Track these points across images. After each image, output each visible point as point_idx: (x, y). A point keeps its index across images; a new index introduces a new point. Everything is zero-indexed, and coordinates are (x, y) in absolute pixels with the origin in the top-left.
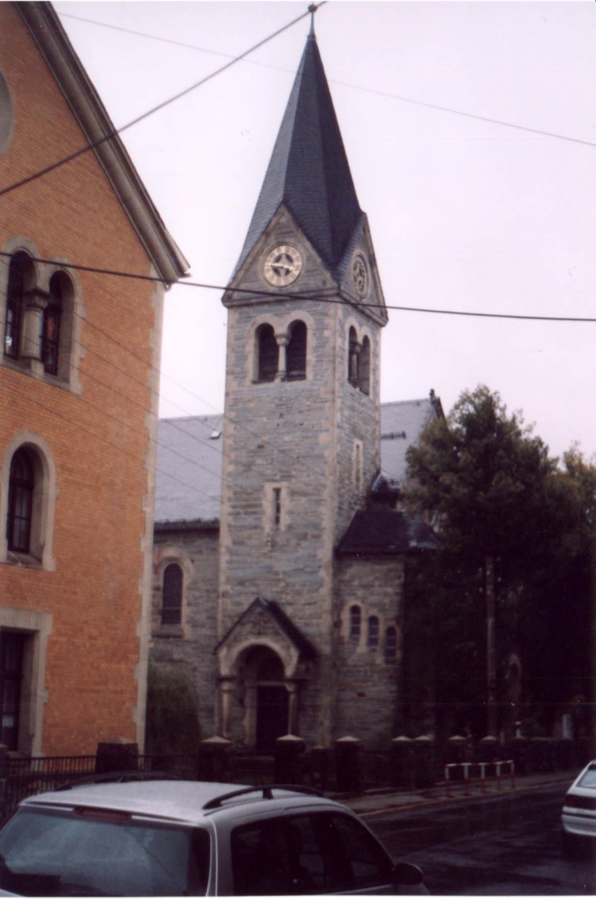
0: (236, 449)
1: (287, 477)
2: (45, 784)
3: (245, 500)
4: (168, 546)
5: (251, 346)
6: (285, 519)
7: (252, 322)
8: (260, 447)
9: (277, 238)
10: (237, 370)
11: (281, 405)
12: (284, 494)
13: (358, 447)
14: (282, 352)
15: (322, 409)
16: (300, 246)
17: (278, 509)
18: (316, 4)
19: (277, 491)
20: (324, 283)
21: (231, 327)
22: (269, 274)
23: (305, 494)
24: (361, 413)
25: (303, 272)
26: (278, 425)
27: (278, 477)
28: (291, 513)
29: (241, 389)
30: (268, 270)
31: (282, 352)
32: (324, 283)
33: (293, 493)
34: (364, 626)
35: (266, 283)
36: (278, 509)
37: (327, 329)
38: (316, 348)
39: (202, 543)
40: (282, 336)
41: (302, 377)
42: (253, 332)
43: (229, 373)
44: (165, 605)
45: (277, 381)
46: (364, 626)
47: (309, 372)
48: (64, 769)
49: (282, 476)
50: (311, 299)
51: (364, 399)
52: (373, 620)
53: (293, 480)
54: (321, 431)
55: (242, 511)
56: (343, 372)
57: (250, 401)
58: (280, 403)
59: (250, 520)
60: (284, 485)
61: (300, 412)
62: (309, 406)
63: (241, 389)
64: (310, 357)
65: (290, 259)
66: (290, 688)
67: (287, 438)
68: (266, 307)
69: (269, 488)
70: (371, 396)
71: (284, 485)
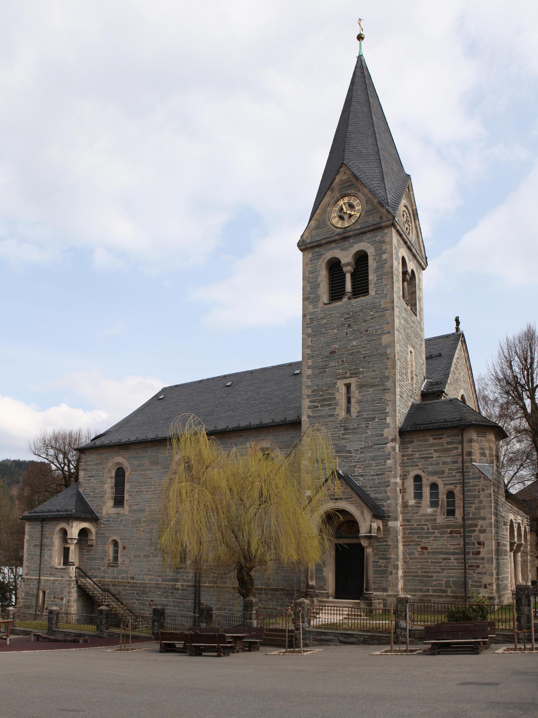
0: (313, 357)
1: (355, 374)
2: (335, 622)
3: (321, 396)
4: (262, 440)
5: (323, 275)
6: (355, 408)
7: (322, 259)
8: (332, 353)
9: (340, 192)
10: (312, 296)
11: (349, 318)
12: (353, 388)
13: (411, 352)
14: (348, 277)
15: (384, 315)
16: (359, 194)
17: (349, 401)
18: (363, 42)
19: (348, 386)
20: (381, 218)
21: (305, 265)
22: (335, 221)
23: (372, 386)
24: (412, 327)
25: (363, 213)
26: (347, 334)
27: (348, 375)
28: (359, 402)
29: (316, 310)
30: (334, 217)
31: (348, 277)
32: (381, 218)
33: (360, 386)
34: (426, 491)
35: (332, 227)
36: (349, 401)
37: (385, 253)
38: (376, 270)
39: (286, 436)
40: (348, 264)
41: (366, 292)
42: (324, 266)
43: (305, 299)
44: (284, 646)
45: (345, 299)
46: (426, 491)
47: (372, 291)
48: (190, 604)
49: (352, 374)
50: (370, 231)
51: (414, 318)
52: (434, 486)
53: (361, 376)
54: (384, 334)
55: (319, 405)
56: (399, 288)
57: (323, 318)
58: (348, 316)
59: (326, 410)
60: (353, 381)
61: (365, 321)
62: (372, 315)
63: (316, 310)
64: (372, 277)
65: (351, 206)
66: (364, 543)
67: (355, 343)
68: (334, 245)
69: (341, 385)
70: (418, 317)
71: (353, 381)
